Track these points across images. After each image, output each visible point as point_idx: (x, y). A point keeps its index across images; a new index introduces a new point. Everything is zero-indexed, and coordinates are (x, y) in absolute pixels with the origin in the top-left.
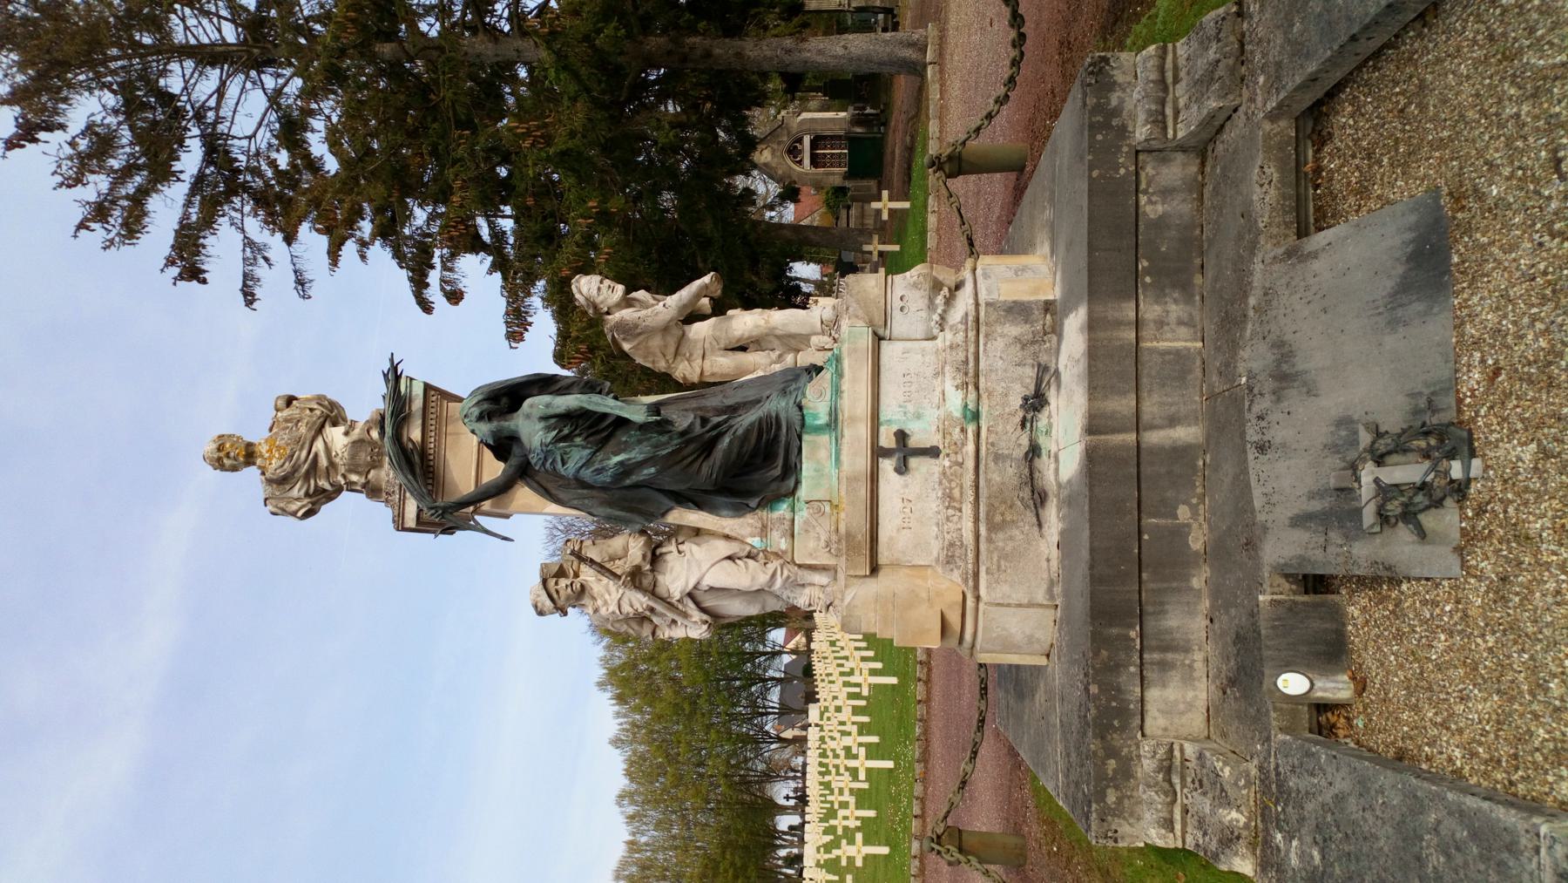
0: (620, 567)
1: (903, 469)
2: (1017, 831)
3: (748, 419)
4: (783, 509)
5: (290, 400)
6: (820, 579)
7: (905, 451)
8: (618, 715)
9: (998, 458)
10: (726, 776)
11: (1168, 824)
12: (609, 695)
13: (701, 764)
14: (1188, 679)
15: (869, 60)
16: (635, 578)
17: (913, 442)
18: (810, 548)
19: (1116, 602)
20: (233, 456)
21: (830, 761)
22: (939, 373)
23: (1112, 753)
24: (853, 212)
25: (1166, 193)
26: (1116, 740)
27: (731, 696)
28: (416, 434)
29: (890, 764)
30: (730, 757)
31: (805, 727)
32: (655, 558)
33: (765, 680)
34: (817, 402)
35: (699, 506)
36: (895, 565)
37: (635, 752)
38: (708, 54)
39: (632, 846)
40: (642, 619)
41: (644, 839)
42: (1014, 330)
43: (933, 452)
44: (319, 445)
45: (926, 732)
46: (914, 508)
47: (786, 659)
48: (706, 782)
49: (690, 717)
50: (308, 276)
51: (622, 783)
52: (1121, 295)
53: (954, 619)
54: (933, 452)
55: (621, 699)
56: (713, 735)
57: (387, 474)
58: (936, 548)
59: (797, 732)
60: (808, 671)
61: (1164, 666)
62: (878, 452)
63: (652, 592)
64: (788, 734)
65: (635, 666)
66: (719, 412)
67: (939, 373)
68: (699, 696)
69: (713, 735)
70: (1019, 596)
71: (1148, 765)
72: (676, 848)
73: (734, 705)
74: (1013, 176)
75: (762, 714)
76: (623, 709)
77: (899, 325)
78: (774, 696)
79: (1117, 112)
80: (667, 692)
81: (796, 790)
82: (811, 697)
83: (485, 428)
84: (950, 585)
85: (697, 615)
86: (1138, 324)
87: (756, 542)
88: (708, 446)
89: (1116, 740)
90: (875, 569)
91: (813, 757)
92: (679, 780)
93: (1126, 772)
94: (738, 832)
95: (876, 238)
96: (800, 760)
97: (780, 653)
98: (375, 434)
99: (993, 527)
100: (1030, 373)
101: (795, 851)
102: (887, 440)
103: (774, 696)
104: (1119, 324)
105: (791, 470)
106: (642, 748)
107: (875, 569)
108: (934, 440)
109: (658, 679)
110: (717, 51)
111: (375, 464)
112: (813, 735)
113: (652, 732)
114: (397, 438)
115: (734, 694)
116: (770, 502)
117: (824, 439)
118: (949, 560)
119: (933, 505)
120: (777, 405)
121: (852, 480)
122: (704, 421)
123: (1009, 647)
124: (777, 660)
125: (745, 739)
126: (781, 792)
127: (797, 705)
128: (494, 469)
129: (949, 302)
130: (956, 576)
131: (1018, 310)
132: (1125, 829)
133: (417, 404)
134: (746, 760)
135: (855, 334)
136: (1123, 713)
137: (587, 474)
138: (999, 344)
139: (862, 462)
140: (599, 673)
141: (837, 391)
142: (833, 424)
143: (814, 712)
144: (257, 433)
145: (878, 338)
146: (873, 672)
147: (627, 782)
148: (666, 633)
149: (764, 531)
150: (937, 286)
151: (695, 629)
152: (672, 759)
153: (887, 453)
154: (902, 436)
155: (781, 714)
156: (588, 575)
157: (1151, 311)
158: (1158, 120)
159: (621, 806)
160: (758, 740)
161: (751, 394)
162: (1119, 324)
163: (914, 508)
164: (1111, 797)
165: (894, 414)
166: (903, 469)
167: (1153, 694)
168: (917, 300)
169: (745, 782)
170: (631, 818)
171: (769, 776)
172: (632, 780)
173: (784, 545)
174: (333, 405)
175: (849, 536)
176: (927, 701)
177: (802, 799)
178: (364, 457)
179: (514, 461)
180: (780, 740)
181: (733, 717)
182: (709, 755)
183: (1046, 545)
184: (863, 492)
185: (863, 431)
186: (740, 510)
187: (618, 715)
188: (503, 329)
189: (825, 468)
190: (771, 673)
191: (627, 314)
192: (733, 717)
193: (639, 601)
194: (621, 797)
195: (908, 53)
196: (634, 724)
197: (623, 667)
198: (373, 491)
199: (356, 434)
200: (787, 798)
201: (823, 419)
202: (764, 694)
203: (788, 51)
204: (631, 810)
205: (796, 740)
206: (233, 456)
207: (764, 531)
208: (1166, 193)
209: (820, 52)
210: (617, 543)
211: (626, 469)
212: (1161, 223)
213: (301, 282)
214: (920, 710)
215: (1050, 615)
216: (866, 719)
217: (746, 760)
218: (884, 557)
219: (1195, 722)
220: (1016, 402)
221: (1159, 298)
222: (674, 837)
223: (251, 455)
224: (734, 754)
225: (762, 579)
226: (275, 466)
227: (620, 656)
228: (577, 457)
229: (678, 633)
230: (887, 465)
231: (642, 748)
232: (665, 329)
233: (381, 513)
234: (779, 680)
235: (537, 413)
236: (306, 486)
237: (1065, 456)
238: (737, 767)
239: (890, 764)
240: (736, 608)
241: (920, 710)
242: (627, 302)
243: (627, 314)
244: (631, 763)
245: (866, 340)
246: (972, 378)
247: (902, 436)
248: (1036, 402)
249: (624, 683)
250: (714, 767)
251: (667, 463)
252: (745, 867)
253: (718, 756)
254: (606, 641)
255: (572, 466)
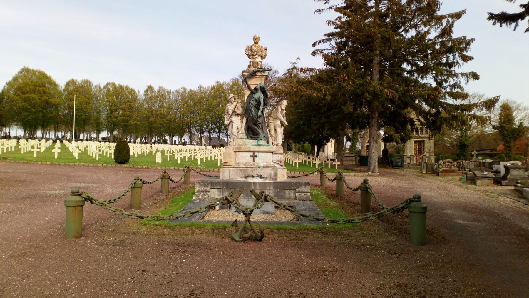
0: (236, 109)
1: (251, 156)
2: (190, 183)
3: (260, 131)
4: (245, 137)
5: (266, 50)
6: (235, 143)
7: (254, 157)
8: (209, 87)
9: (252, 171)
10: (191, 121)
11: (199, 191)
12: (214, 85)
13: (194, 113)
14: (218, 195)
15: (371, 158)
16: (234, 112)
17: (255, 158)
18: (239, 141)
19: (228, 185)
20: (256, 40)
21: (193, 152)
22: (266, 162)
23: (208, 184)
24: (354, 158)
25: (289, 194)
26: (210, 185)
27: (215, 122)
28: (259, 74)
29: (199, 164)
30: (196, 122)
31: (205, 145)
32: (238, 115)
33: (219, 132)
34: (262, 142)
35: (246, 123)
36: (236, 155)
37: (198, 93)
38: (373, 118)
39: (169, 92)
40: (228, 113)
41: (171, 96)
42: (273, 174)
43: (254, 161)
44: (257, 56)
45: (207, 171)
46: (245, 158)
47: (226, 139)
48: (189, 115)
49: (209, 110)
50: (321, 12)
51: (188, 89)
52: (274, 187)
53: (227, 164)
54: (254, 161)
55: (213, 88)
56: (203, 117)
57: (252, 69)
58: (238, 161)
59: (204, 142)
60: (222, 146)
61: (220, 192)
62: (254, 152)
63: (232, 115)
64: (203, 140)
65: (223, 93)
66: (262, 126)
67: (266, 162)
68: (214, 112)
69: (203, 117)
70: (231, 174)
71: (206, 188)
72: (169, 105)
73: (212, 123)
74: (319, 183)
75: (209, 132)
76: (210, 89)
77: (275, 156)
78: (214, 136)
79: (301, 186)
80: (215, 103)
81: (186, 142)
82: (214, 147)
83: (258, 87)
84: (233, 164)
85: (228, 122)
86: (270, 189)
87: (240, 132)
88: (255, 125)
89: (210, 185)
90: (235, 152)
91: (197, 147)
92: (189, 106)
93: (205, 186)
94: (174, 124)
95: (339, 163)
96: (195, 144)
97: (227, 137)
98: (259, 67)
99: (241, 170)
100: (266, 176)
101: (168, 142)
102: (256, 154)
103: (214, 136)
104: (270, 187)
105: (252, 138)
106: (199, 95)
107: (235, 152)
108: (256, 161)
109: (219, 100)
110: (374, 120)
111: (254, 67)
112: (203, 147)
113: (203, 98)
114: (258, 71)
115: (215, 123)
116: (247, 135)
117: (256, 144)
118: (236, 163)
119: (245, 161)
120: (262, 136)
121: (249, 148)
122: (260, 124)
123: (223, 173)
124: (225, 136)
125: (201, 127)
126: (186, 138)
127: (212, 143)
128: (253, 87)
129: (278, 164)
130: (234, 164)
131: (276, 174)
132: (198, 185)
133: (264, 74)
134: (195, 127)
135: (272, 148)
136: (213, 186)
137: (251, 104)
138: (271, 171)
139: (252, 150)
140: (221, 82)
141: (264, 146)
142: (258, 145)
143: (210, 148)
144: (260, 43)
145: (273, 152)
146: (221, 160)
147: (189, 90)
148: (225, 117)
149: (242, 134)
150: (281, 162)
151: (226, 122)
152: (195, 104)
153: (254, 154)
154: (256, 156)
155: (209, 137)
156: (235, 104)
157: (272, 191)
158: (299, 192)
159: (182, 88)
160: (202, 132)
161: (265, 131)
162: (270, 187)
163: (245, 158)
164: (202, 184)
165: (260, 155)
166: (251, 156)
167: (216, 190)
168: (278, 159)
169: (188, 127)
170: (178, 92)
171: (191, 135)
172: (189, 92)
173: (240, 137)
174: (265, 57)
175: (240, 148)
176: (214, 172)
177: (184, 144)
178: (255, 65)
179: (254, 91)
180: (201, 137)
181: (208, 123)
182: (197, 116)
183: (239, 178)
184: (247, 150)
185: (257, 150)
186: (245, 130)
187: (209, 87)
188: (304, 67)
189: (251, 144)
190: (221, 134)
191: (280, 110)
192: (208, 123)
193: (230, 113)
194: (184, 88)
195: (372, 168)
196: (206, 92)
197: (223, 89)
198: (249, 66)
199: (259, 63)
200: (184, 140)
201: (259, 143)
202: (215, 132)
203: (373, 138)
204: (180, 92)
205: (201, 142)
206: (256, 40)
207: (242, 134)
208: (289, 194)
209: (373, 146)
210: (240, 109)
211: (251, 111)
212: (285, 193)
213: (320, 11)
214: (212, 170)
215: (228, 179)
216: (209, 159)
217: (195, 127)
218: (237, 153)
219: (212, 196)
220: (261, 174)
221: (273, 192)
222: (172, 105)
223: (256, 43)
224: (197, 123)
225: (234, 134)
226: (254, 48)
227: (226, 88)
228: (253, 103)
229: (225, 119)
230: (252, 154)
231: (199, 95)
232: (277, 116)
233: (246, 68)
234: (219, 137)
235: (261, 97)
236: (251, 53)
237: (250, 180)
238: (193, 124)
239: (199, 164)
240: (230, 129)
241: (212, 170)
242: (282, 110)
243: (280, 110)
244: (194, 91)
245: (272, 150)
246: (265, 167)
247: (256, 156)
248: (261, 177)
249: (218, 89)
250: (193, 117)
251: (252, 118)
252: (164, 127)
253: (197, 118)
254: (231, 84)
255: (252, 102)
